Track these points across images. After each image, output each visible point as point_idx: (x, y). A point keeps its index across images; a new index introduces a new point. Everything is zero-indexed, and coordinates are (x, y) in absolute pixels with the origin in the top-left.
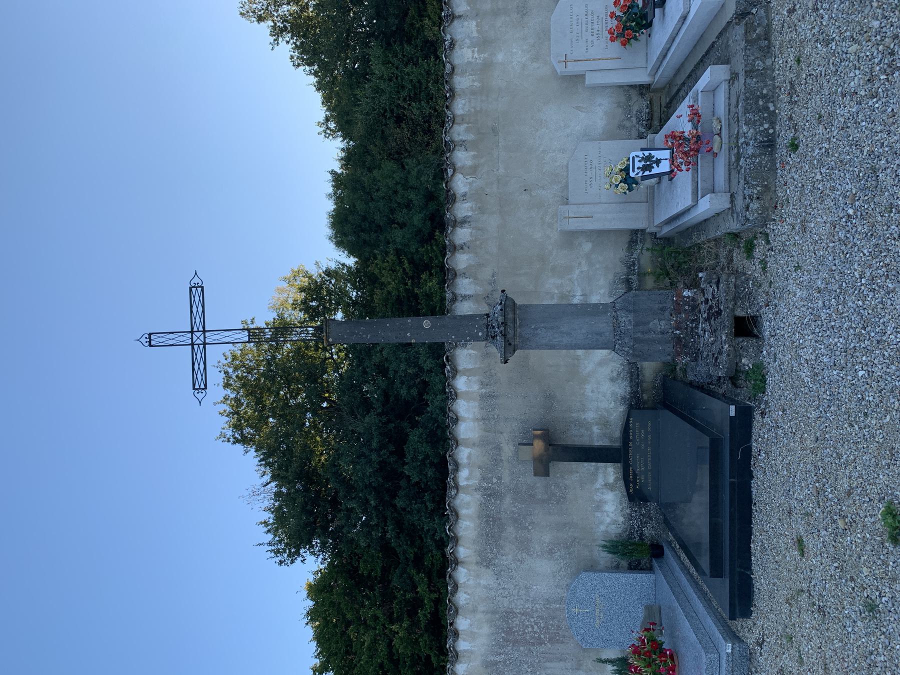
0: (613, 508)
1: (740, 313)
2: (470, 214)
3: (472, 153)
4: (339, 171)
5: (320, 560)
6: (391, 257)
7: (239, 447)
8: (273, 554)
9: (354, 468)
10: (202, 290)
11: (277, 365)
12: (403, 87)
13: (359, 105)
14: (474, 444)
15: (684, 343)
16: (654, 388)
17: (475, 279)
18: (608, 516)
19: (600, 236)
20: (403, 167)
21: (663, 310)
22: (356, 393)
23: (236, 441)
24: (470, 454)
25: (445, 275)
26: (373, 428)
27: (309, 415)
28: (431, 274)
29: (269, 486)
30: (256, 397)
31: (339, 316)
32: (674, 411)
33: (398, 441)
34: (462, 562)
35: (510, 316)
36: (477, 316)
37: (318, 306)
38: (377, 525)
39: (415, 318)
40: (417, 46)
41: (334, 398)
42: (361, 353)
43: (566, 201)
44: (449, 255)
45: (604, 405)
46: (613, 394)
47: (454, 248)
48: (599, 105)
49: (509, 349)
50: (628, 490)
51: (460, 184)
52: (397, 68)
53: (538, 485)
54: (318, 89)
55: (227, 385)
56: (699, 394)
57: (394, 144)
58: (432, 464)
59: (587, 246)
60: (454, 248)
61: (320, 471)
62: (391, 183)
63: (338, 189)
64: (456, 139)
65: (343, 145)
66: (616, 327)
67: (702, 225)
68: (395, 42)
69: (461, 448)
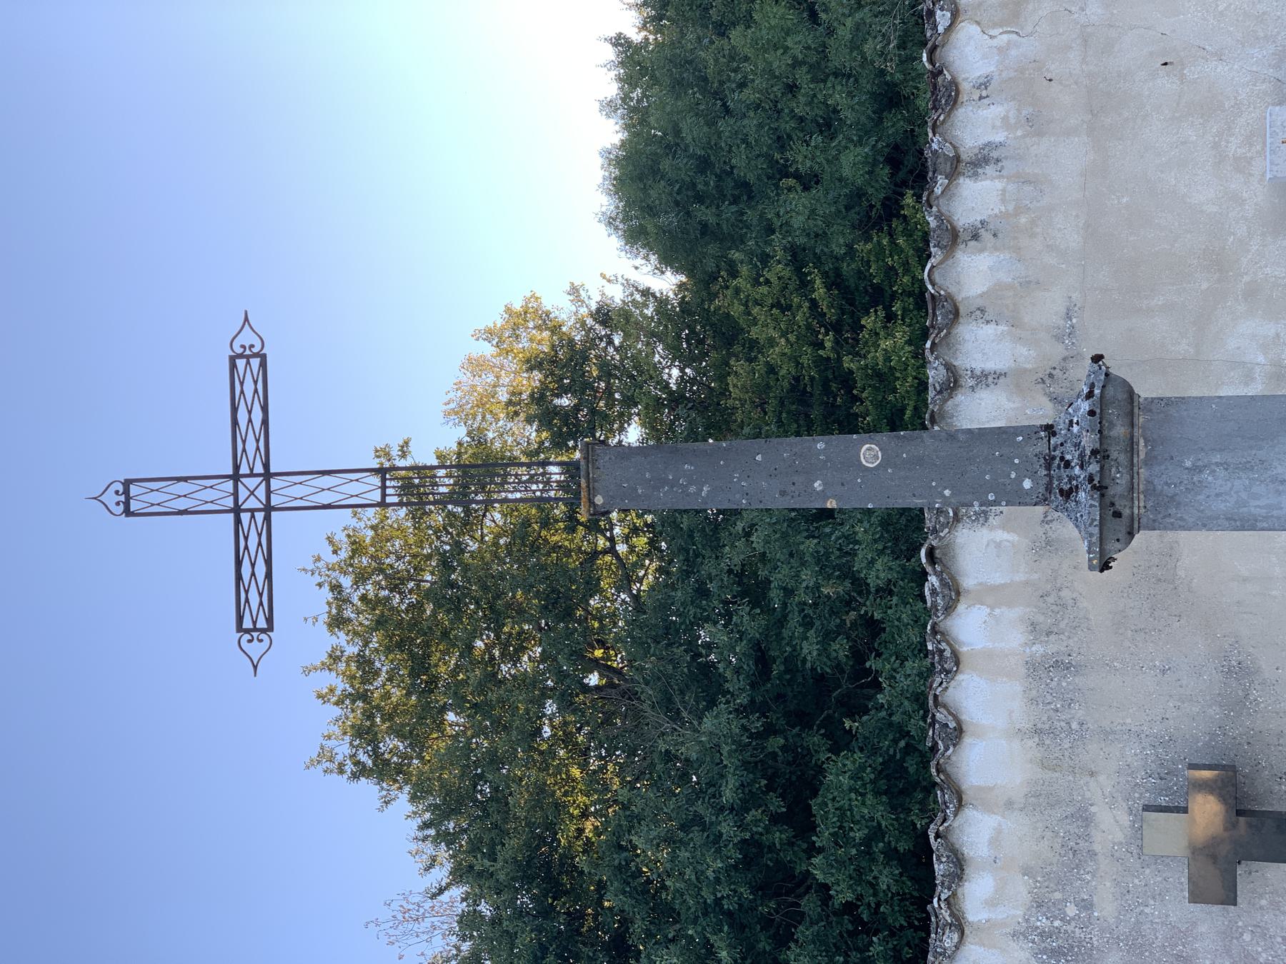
2: (999, 137)
4: (636, 37)
6: (778, 270)
7: (368, 789)
9: (673, 858)
10: (263, 365)
11: (466, 568)
14: (1009, 804)
20: (813, 16)
22: (679, 651)
23: (361, 771)
24: (999, 831)
25: (925, 313)
26: (725, 749)
27: (550, 707)
28: (890, 317)
29: (445, 897)
30: (412, 656)
31: (633, 434)
33: (795, 790)
35: (1119, 430)
36: (1016, 431)
37: (577, 408)
39: (838, 439)
42: (691, 538)
47: (953, 238)
49: (1115, 526)
53: (1203, 928)
55: (337, 622)
58: (892, 854)
60: (953, 238)
61: (581, 861)
62: (779, 63)
63: (633, 86)
69: (968, 813)
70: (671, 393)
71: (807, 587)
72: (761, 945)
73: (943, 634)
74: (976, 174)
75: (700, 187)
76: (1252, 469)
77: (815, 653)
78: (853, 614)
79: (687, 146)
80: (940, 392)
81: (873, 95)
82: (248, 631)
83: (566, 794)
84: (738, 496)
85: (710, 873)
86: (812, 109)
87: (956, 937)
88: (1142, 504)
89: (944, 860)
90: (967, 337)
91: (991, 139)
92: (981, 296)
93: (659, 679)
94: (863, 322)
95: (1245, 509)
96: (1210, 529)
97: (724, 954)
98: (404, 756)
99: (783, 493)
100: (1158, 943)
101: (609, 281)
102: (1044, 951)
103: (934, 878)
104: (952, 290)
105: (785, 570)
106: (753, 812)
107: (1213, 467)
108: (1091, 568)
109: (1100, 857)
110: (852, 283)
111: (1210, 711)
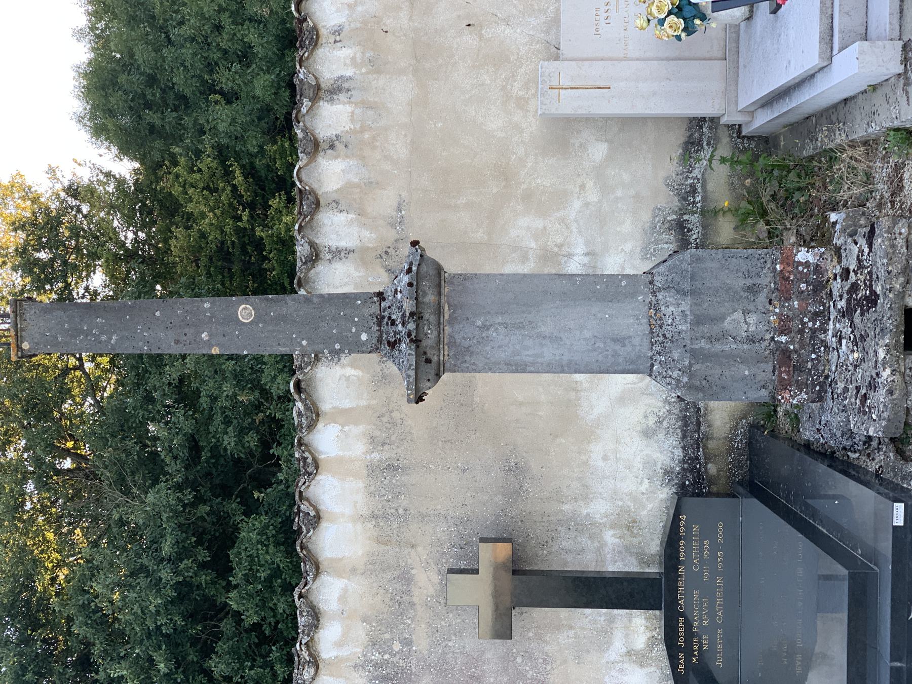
2: (349, 73)
6: (208, 162)
14: (354, 570)
15: (796, 363)
16: (731, 449)
17: (361, 213)
19: (628, 125)
21: (753, 290)
24: (345, 590)
26: (165, 516)
31: (98, 280)
35: (430, 298)
36: (356, 296)
37: (52, 260)
41: (85, 450)
43: (555, 53)
44: (303, 159)
46: (648, 463)
47: (316, 147)
49: (426, 369)
50: (674, 666)
53: (488, 655)
56: (822, 468)
59: (598, 151)
66: (655, 324)
67: (839, 111)
69: (324, 578)
70: (126, 250)
71: (227, 396)
72: (190, 658)
73: (306, 445)
74: (332, 100)
75: (148, 97)
76: (524, 328)
77: (233, 444)
78: (261, 415)
79: (139, 66)
80: (305, 263)
81: (277, 37)
83: (42, 552)
84: (140, 344)
85: (152, 608)
86: (233, 44)
87: (312, 671)
88: (446, 353)
89: (305, 614)
90: (326, 222)
91: (344, 74)
92: (336, 191)
93: (115, 464)
94: (270, 203)
95: (518, 357)
96: (494, 372)
97: (162, 665)
99: (177, 342)
100: (457, 667)
101: (80, 164)
102: (376, 678)
103: (297, 628)
104: (315, 186)
105: (211, 383)
106: (185, 561)
107: (497, 326)
108: (409, 401)
109: (418, 607)
110: (263, 173)
111: (496, 499)
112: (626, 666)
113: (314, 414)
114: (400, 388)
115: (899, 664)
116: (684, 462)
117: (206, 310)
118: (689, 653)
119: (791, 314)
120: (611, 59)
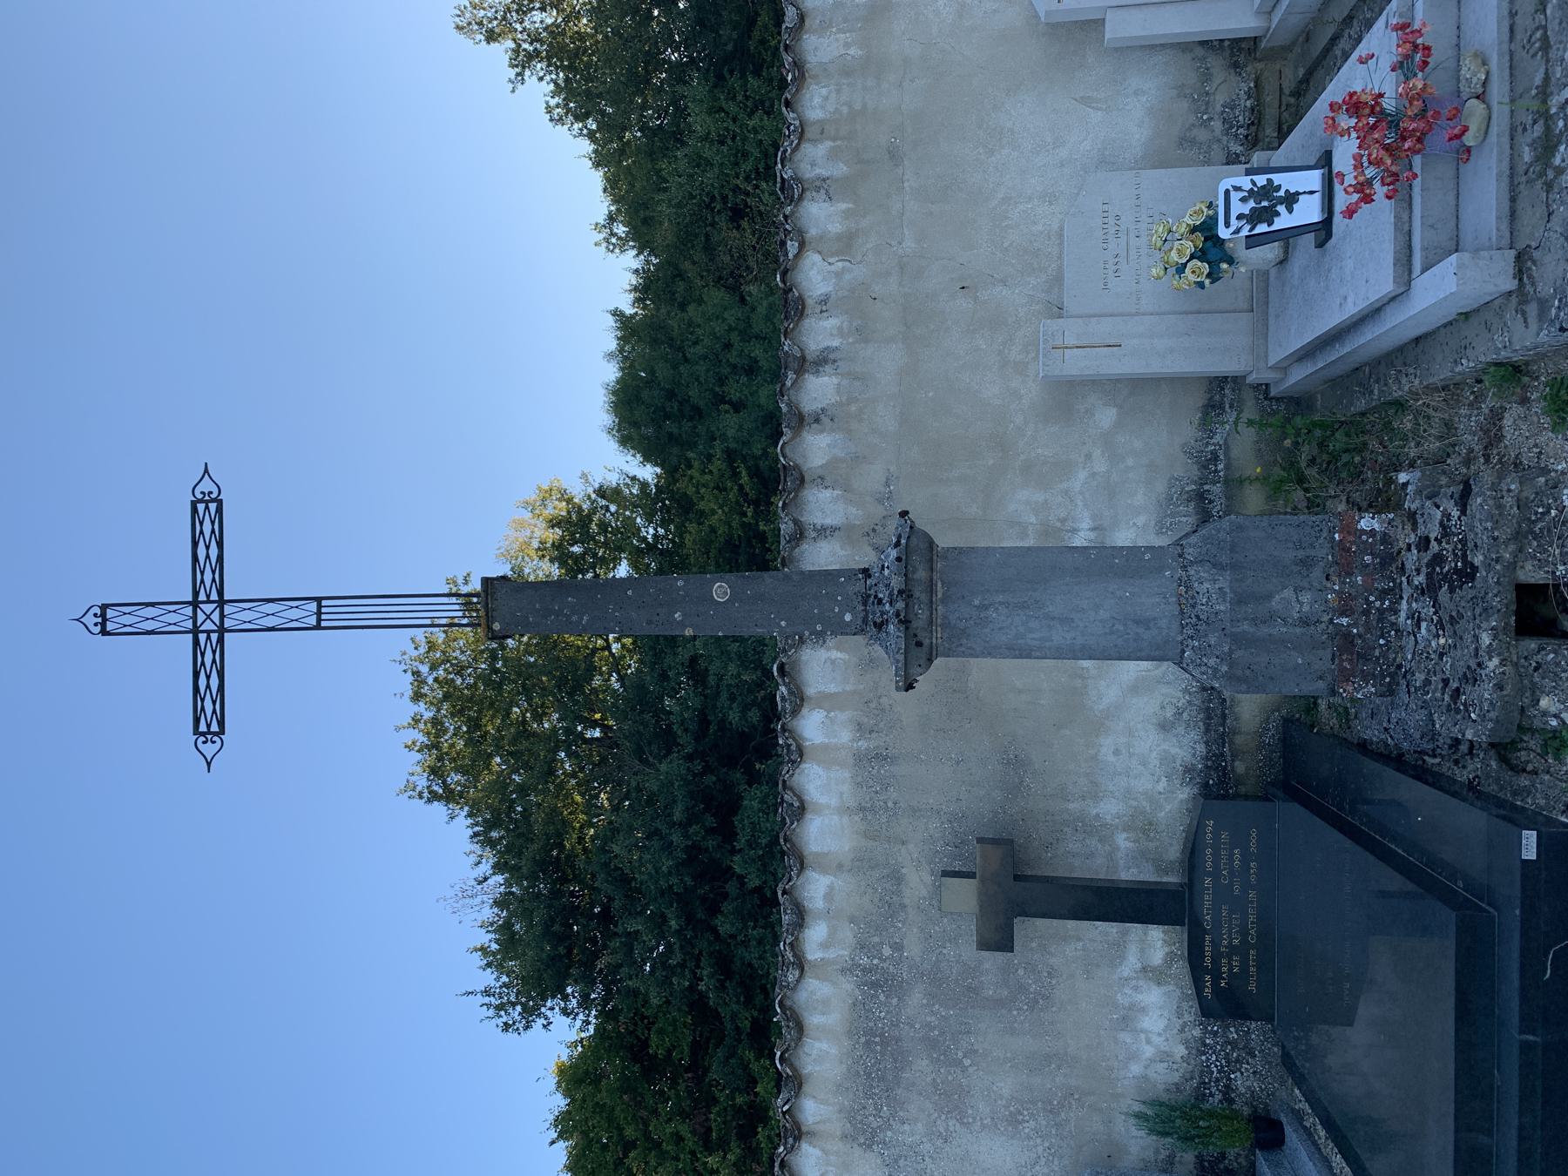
0: (1162, 1024)
1: (1531, 574)
2: (835, 343)
3: (843, 206)
4: (629, 311)
5: (578, 1023)
6: (718, 464)
7: (439, 808)
8: (491, 1012)
12: (745, 155)
13: (665, 190)
14: (840, 866)
18: (1148, 1042)
19: (1136, 390)
20: (743, 300)
21: (1306, 563)
23: (434, 797)
31: (623, 570)
32: (1306, 803)
34: (811, 1134)
35: (921, 574)
36: (839, 573)
38: (682, 965)
40: (771, 80)
43: (1058, 311)
44: (787, 434)
45: (1143, 784)
46: (1166, 759)
47: (800, 421)
48: (1136, 93)
51: (815, 276)
52: (735, 120)
53: (987, 966)
54: (597, 165)
55: (417, 697)
56: (1389, 773)
57: (727, 259)
59: (1106, 416)
62: (719, 328)
64: (807, 176)
65: (637, 264)
68: (731, 72)
74: (818, 372)
82: (203, 734)
87: (797, 973)
98: (464, 786)
99: (649, 622)
104: (799, 461)
108: (898, 689)
109: (910, 910)
112: (1141, 983)
113: (799, 699)
114: (888, 675)
115: (1531, 1038)
116: (1207, 759)
117: (679, 589)
118: (1217, 978)
119: (1353, 591)
120: (1122, 315)
